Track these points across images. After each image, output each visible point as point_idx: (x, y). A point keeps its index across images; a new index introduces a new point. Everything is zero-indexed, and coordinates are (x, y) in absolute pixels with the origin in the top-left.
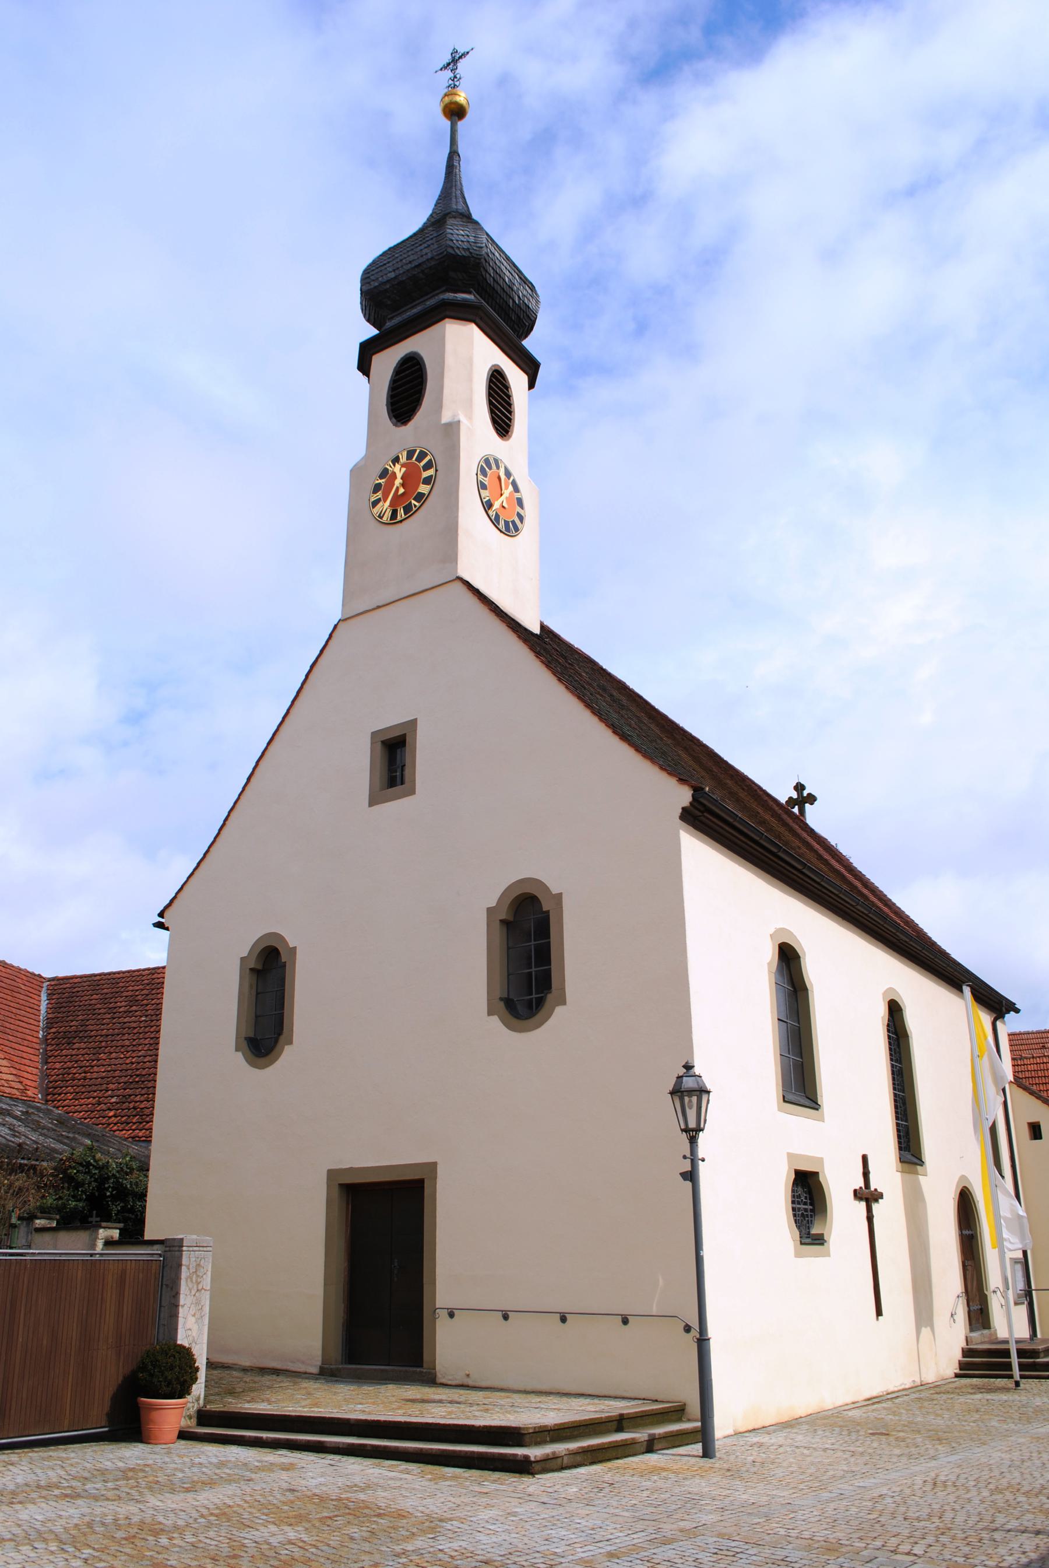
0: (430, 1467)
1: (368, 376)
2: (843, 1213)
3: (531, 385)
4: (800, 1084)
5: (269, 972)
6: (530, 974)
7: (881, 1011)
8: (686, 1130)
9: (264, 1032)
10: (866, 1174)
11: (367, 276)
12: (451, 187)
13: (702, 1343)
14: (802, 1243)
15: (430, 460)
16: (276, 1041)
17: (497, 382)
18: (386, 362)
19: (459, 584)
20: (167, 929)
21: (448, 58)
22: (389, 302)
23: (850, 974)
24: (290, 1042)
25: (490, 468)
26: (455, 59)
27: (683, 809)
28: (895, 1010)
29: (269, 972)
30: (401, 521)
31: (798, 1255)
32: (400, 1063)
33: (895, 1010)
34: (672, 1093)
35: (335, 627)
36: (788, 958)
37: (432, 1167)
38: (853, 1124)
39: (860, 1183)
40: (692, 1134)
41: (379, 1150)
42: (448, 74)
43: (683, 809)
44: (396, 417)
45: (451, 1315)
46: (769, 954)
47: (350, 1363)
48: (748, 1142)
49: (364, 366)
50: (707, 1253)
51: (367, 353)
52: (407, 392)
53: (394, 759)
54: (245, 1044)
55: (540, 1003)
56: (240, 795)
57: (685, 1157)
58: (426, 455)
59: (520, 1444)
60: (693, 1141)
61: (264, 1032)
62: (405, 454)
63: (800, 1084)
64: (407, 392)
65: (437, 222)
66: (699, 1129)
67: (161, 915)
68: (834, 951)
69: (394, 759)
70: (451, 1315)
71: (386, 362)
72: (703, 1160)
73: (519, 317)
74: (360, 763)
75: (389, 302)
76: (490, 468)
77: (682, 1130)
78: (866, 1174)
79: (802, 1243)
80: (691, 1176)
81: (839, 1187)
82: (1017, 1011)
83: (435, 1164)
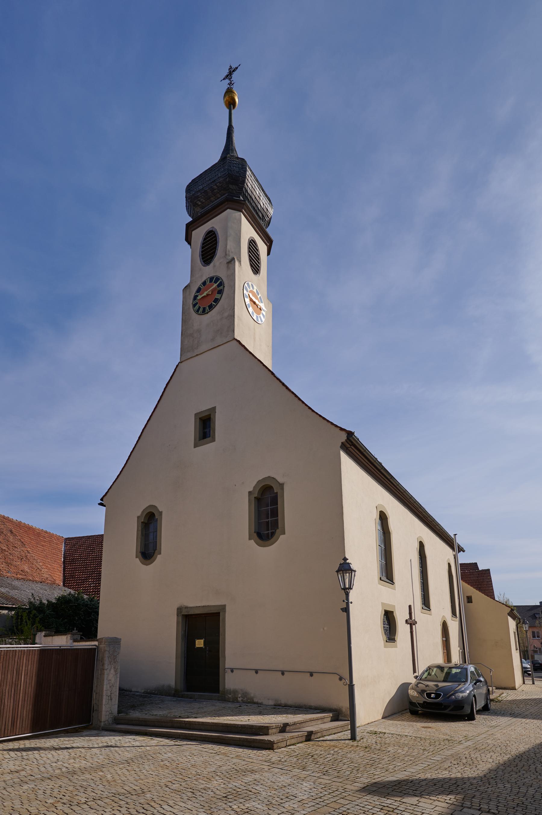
0: (271, 349)
1: (190, 245)
2: (402, 629)
3: (269, 254)
4: (387, 574)
5: (150, 522)
6: (268, 522)
7: (417, 546)
8: (345, 589)
9: (148, 552)
10: (410, 614)
11: (189, 189)
12: (229, 145)
13: (351, 687)
14: (387, 641)
15: (221, 282)
16: (154, 553)
17: (252, 243)
18: (199, 234)
19: (235, 342)
20: (105, 506)
21: (226, 72)
22: (200, 203)
23: (406, 529)
24: (160, 553)
25: (250, 288)
26: (232, 71)
27: (342, 443)
28: (422, 545)
29: (150, 522)
30: (207, 313)
31: (385, 647)
32: (209, 559)
33: (422, 545)
34: (337, 572)
35: (177, 366)
36: (383, 518)
37: (223, 608)
38: (403, 594)
39: (408, 617)
40: (346, 591)
41: (198, 600)
42: (227, 81)
43: (342, 443)
44: (204, 262)
45: (232, 671)
46: (376, 515)
47: (187, 692)
48: (367, 598)
49: (188, 239)
50: (353, 646)
51: (190, 228)
52: (209, 250)
53: (205, 427)
54: (140, 555)
55: (273, 534)
56: (135, 445)
57: (344, 601)
58: (219, 279)
59: (267, 734)
60: (347, 595)
61: (148, 552)
62: (209, 280)
63: (387, 574)
64: (209, 250)
65: (223, 158)
66: (350, 588)
67: (102, 500)
68: (400, 518)
69: (205, 427)
70: (232, 671)
71: (199, 234)
72: (351, 603)
73: (263, 216)
74: (190, 429)
75: (200, 203)
76: (250, 288)
77: (342, 589)
78: (410, 614)
79: (387, 641)
80: (346, 610)
81: (401, 617)
82: (464, 551)
83: (225, 605)
